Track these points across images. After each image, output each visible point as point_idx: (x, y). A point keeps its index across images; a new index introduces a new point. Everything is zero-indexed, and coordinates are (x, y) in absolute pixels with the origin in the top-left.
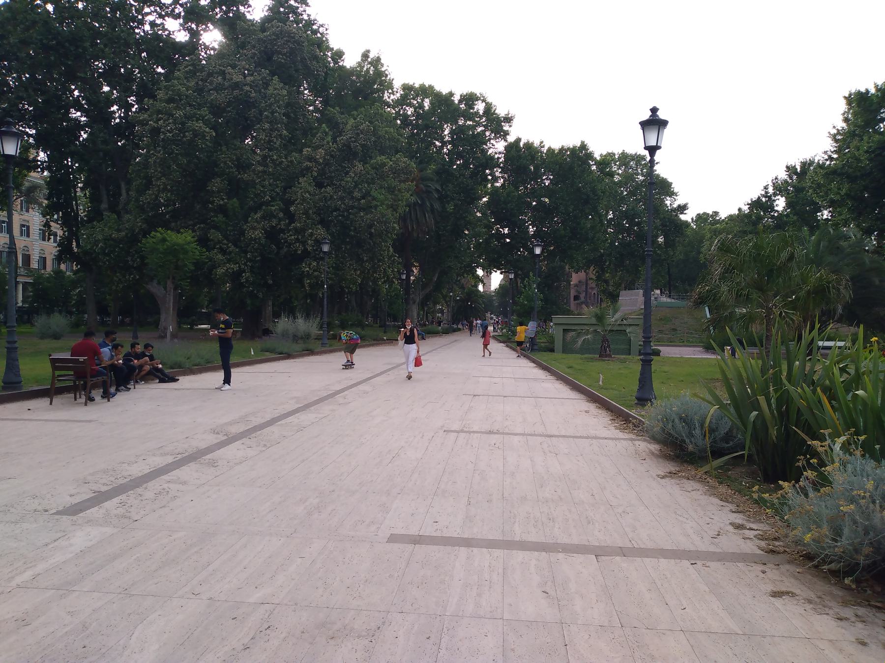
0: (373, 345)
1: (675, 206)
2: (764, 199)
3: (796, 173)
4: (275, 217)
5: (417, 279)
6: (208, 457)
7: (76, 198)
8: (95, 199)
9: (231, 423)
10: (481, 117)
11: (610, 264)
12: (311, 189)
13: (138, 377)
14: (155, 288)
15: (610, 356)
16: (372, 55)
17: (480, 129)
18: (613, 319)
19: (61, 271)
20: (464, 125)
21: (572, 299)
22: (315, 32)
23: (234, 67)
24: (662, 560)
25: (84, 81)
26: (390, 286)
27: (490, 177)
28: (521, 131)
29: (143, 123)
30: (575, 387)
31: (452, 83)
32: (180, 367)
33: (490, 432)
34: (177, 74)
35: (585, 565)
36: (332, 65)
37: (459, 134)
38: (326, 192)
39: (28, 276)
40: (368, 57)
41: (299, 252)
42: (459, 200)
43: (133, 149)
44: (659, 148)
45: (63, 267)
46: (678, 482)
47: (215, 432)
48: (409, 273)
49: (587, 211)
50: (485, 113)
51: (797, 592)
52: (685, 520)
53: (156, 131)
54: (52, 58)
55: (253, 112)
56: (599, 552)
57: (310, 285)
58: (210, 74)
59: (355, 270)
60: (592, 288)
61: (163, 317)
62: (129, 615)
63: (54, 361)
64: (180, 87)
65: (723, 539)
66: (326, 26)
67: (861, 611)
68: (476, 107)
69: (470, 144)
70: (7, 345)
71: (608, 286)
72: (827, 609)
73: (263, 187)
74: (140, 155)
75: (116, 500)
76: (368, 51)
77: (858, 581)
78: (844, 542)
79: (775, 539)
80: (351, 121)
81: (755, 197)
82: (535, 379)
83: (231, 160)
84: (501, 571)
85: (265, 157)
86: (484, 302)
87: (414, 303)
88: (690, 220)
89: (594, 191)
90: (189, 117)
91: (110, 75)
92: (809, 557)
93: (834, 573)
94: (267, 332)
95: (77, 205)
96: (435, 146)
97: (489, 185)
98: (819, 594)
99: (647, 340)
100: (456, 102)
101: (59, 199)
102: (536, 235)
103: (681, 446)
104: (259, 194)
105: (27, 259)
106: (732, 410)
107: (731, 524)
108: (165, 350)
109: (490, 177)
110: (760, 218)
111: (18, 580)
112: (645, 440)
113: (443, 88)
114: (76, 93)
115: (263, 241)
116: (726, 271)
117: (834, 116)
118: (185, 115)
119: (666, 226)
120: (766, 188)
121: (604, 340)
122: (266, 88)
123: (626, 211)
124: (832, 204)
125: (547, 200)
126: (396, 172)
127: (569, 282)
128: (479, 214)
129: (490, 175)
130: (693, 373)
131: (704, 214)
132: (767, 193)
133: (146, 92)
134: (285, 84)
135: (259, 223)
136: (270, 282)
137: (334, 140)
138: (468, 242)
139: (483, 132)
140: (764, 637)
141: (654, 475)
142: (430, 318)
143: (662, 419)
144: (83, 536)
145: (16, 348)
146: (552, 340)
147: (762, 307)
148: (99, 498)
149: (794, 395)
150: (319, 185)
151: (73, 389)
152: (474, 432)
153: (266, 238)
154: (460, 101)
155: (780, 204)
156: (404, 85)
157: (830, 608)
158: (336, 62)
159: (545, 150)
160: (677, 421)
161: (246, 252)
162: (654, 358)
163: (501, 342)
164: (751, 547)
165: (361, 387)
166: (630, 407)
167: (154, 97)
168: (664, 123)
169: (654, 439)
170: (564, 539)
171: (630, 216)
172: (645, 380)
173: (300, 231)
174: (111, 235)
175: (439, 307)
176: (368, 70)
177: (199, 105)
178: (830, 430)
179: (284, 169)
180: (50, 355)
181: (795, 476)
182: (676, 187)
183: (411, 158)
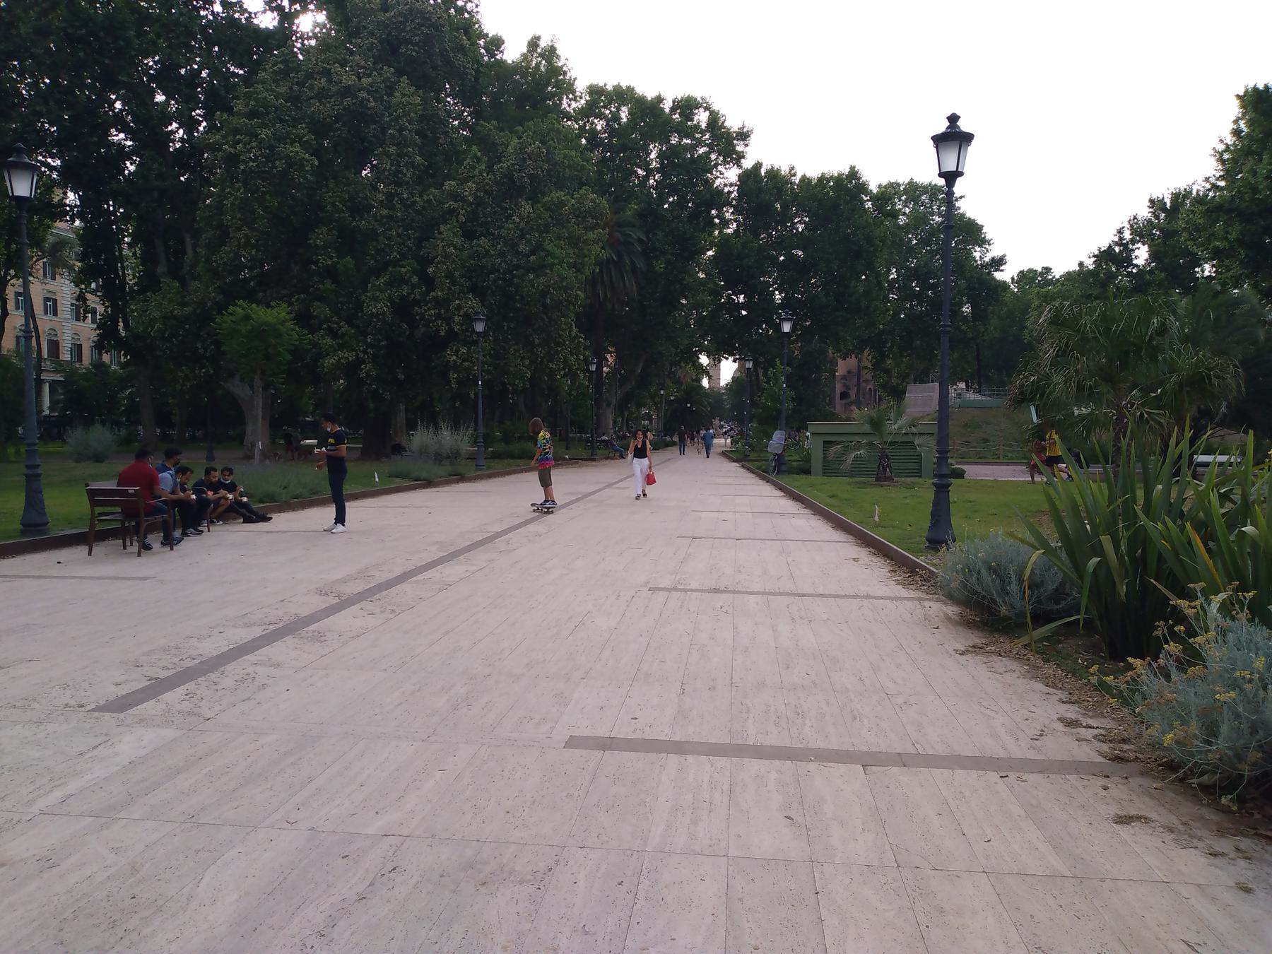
1: (987, 259)
3: (1164, 209)
4: (406, 282)
5: (614, 371)
7: (121, 259)
8: (148, 259)
9: (344, 581)
10: (703, 132)
11: (892, 346)
14: (238, 388)
15: (891, 479)
16: (543, 44)
17: (702, 150)
18: (894, 426)
19: (103, 364)
20: (679, 145)
23: (343, 64)
27: (717, 221)
28: (763, 152)
29: (213, 148)
30: (840, 525)
31: (661, 83)
33: (716, 591)
34: (262, 75)
35: (848, 778)
36: (486, 58)
38: (479, 245)
39: (57, 372)
40: (538, 46)
44: (961, 174)
45: (106, 358)
47: (321, 592)
48: (601, 361)
50: (709, 125)
51: (1153, 816)
52: (993, 714)
53: (232, 160)
54: (81, 54)
56: (868, 760)
57: (459, 382)
58: (309, 76)
59: (523, 359)
60: (867, 381)
61: (249, 429)
62: (197, 852)
63: (92, 494)
64: (266, 94)
65: (1048, 741)
67: (1245, 843)
68: (696, 118)
69: (688, 173)
71: (890, 377)
72: (1195, 841)
73: (388, 239)
74: (211, 195)
75: (180, 690)
76: (538, 38)
77: (1241, 800)
79: (1124, 741)
81: (1104, 245)
84: (726, 787)
85: (390, 196)
86: (709, 403)
87: (609, 405)
89: (869, 239)
90: (281, 139)
91: (166, 78)
92: (1172, 766)
94: (398, 449)
95: (123, 268)
96: (637, 176)
97: (716, 232)
99: (943, 457)
100: (667, 110)
101: (97, 261)
102: (785, 304)
103: (990, 608)
105: (55, 346)
106: (1064, 556)
107: (1059, 719)
108: (252, 476)
109: (717, 221)
110: (1112, 276)
112: (938, 600)
113: (647, 90)
115: (389, 318)
116: (1063, 353)
120: (1120, 232)
121: (883, 456)
122: (390, 95)
124: (1216, 255)
125: (800, 253)
127: (833, 372)
128: (701, 275)
129: (717, 217)
130: (1007, 503)
131: (1031, 270)
132: (1121, 239)
133: (217, 102)
134: (418, 88)
135: (382, 291)
136: (401, 377)
137: (490, 168)
138: (687, 316)
139: (707, 154)
140: (1103, 880)
141: (951, 651)
143: (963, 570)
144: (133, 741)
145: (39, 475)
146: (807, 459)
148: (156, 688)
150: (469, 235)
152: (692, 590)
154: (673, 110)
155: (1141, 254)
157: (1200, 839)
158: (493, 56)
159: (797, 179)
160: (984, 572)
161: (365, 334)
164: (1088, 753)
166: (917, 552)
167: (230, 110)
168: (968, 138)
169: (951, 598)
170: (820, 744)
171: (921, 275)
172: (940, 514)
174: (172, 312)
175: (644, 411)
176: (538, 65)
177: (294, 120)
179: (418, 212)
181: (1149, 649)
182: (988, 232)
183: (602, 192)
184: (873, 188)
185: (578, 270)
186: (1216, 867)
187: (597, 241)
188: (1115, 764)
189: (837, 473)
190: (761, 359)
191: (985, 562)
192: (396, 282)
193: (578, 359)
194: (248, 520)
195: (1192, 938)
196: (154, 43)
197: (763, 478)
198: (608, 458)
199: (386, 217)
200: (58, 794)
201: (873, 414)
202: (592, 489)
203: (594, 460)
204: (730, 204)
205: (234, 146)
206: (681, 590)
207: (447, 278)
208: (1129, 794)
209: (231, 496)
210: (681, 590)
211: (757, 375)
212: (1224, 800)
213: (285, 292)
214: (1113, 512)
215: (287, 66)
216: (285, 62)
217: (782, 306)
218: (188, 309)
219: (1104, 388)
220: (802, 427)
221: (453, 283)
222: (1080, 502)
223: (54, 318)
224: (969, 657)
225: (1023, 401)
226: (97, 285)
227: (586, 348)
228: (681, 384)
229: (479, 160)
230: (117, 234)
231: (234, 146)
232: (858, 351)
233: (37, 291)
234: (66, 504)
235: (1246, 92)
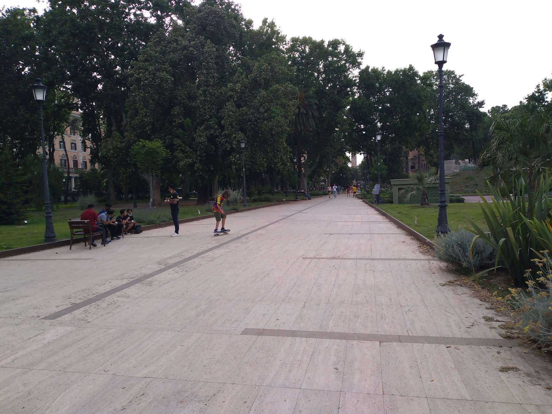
0: (276, 205)
2: (537, 94)
4: (212, 128)
8: (109, 125)
9: (171, 258)
11: (433, 144)
15: (428, 204)
16: (269, 21)
19: (95, 169)
21: (410, 168)
22: (233, 10)
23: (183, 36)
24: (426, 345)
28: (369, 61)
30: (400, 226)
31: (323, 35)
33: (334, 258)
35: (369, 349)
38: (243, 110)
40: (267, 22)
41: (228, 149)
44: (445, 62)
46: (453, 288)
47: (159, 263)
50: (345, 52)
51: (521, 367)
52: (451, 315)
53: (138, 80)
56: (382, 339)
57: (236, 169)
58: (169, 42)
59: (263, 158)
60: (423, 161)
63: (71, 224)
65: (475, 329)
66: (240, 5)
68: (339, 48)
69: (337, 72)
70: (46, 215)
72: (540, 381)
73: (204, 110)
75: (82, 309)
76: (267, 19)
80: (257, 64)
81: (530, 93)
84: (310, 353)
85: (204, 91)
86: (351, 174)
87: (304, 177)
89: (419, 97)
90: (158, 70)
91: (112, 48)
92: (534, 341)
101: (89, 126)
103: (458, 263)
104: (202, 115)
105: (76, 163)
106: (492, 239)
107: (483, 317)
110: (535, 107)
113: (317, 38)
115: (206, 143)
116: (501, 143)
118: (155, 69)
120: (538, 86)
121: (424, 194)
122: (203, 48)
127: (407, 158)
128: (345, 117)
129: (350, 91)
130: (476, 211)
131: (497, 107)
135: (203, 132)
136: (212, 169)
138: (339, 136)
139: (345, 63)
140: (487, 402)
142: (317, 185)
143: (445, 246)
147: (526, 165)
148: (75, 307)
149: (529, 225)
150: (239, 106)
151: (84, 240)
152: (322, 258)
153: (208, 141)
154: (328, 45)
156: (292, 38)
157: (543, 380)
158: (248, 28)
159: (385, 72)
161: (196, 151)
164: (494, 334)
165: (259, 232)
166: (432, 238)
167: (136, 59)
168: (448, 45)
169: (441, 259)
170: (363, 331)
172: (442, 220)
173: (228, 136)
176: (267, 30)
177: (164, 62)
179: (217, 98)
182: (476, 90)
184: (421, 74)
185: (286, 118)
186: (549, 395)
187: (294, 105)
188: (507, 340)
191: (456, 242)
192: (209, 128)
193: (287, 157)
197: (370, 206)
198: (303, 200)
199: (203, 100)
201: (418, 175)
203: (297, 201)
205: (138, 75)
206: (317, 258)
207: (229, 125)
208: (509, 356)
210: (317, 258)
211: (371, 162)
213: (163, 135)
215: (160, 39)
216: (159, 37)
219: (521, 158)
224: (446, 287)
227: (290, 152)
229: (242, 74)
231: (138, 75)
232: (418, 145)
233: (68, 140)
234: (62, 229)
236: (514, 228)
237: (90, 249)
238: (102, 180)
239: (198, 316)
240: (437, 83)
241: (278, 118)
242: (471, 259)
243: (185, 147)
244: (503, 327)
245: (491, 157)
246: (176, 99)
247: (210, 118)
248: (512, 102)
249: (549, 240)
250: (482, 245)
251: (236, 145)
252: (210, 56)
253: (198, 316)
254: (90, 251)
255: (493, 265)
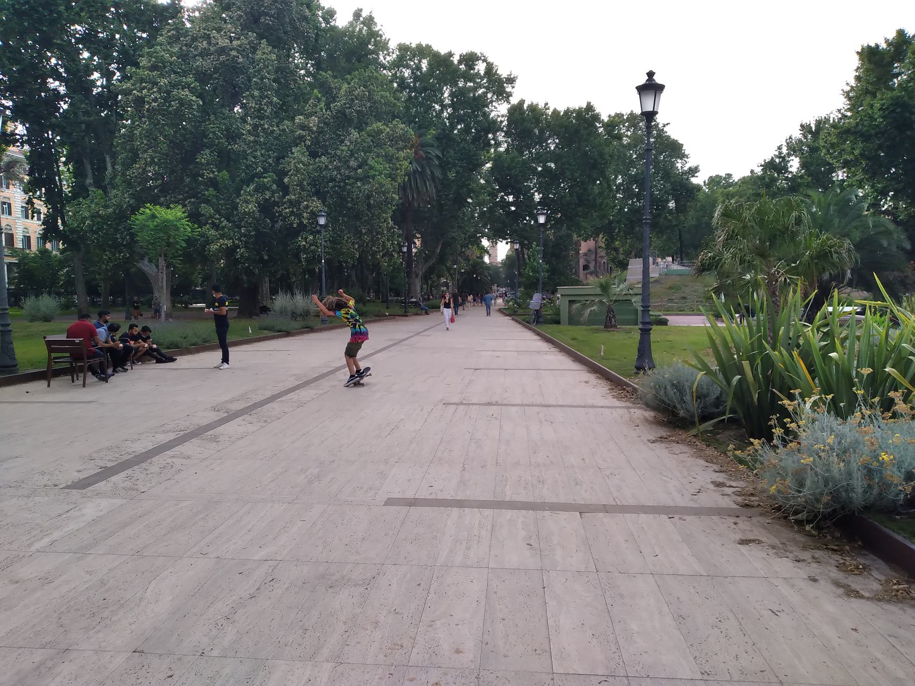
1: (686, 169)
3: (810, 132)
5: (420, 252)
6: (210, 433)
7: (59, 173)
8: (78, 173)
9: (231, 401)
11: (619, 232)
12: (305, 159)
13: (135, 358)
14: (146, 266)
15: (615, 326)
16: (364, 14)
17: (481, 91)
18: (617, 289)
19: (46, 251)
20: (464, 87)
23: (219, 30)
25: (61, 48)
26: (390, 260)
27: (493, 142)
28: (525, 93)
29: (127, 93)
31: (451, 43)
32: (177, 346)
33: (489, 404)
34: (160, 39)
35: (568, 521)
36: (323, 25)
37: (460, 97)
38: (320, 162)
39: (12, 256)
41: (295, 226)
42: (461, 166)
43: (117, 120)
45: (48, 246)
47: (215, 409)
48: (411, 243)
49: (595, 176)
50: (486, 73)
51: (764, 539)
52: (669, 480)
53: (140, 101)
54: (26, 24)
55: (241, 79)
56: (582, 509)
58: (194, 39)
60: (602, 257)
61: (156, 294)
62: (143, 573)
63: (49, 343)
64: (163, 53)
67: (818, 554)
68: (476, 67)
69: (471, 107)
71: (617, 254)
73: (255, 157)
74: (125, 126)
75: (122, 475)
76: (361, 10)
77: (818, 528)
78: (806, 491)
79: (752, 495)
82: (538, 352)
83: (221, 130)
84: (489, 527)
85: (255, 127)
86: (490, 275)
87: (417, 276)
88: (702, 184)
89: (601, 155)
90: (174, 86)
91: (88, 40)
92: (779, 509)
93: (800, 523)
94: (265, 310)
95: (60, 180)
97: (492, 150)
98: (784, 541)
100: (456, 62)
101: (41, 177)
105: (10, 238)
106: (721, 376)
108: (164, 329)
109: (493, 142)
110: (774, 180)
111: (37, 546)
113: (442, 49)
114: (53, 61)
117: (846, 71)
119: (677, 190)
120: (780, 148)
121: (610, 310)
122: (254, 53)
123: (637, 174)
124: (846, 164)
125: (553, 165)
126: (393, 140)
128: (482, 181)
129: (493, 139)
131: (717, 176)
132: (780, 153)
133: (128, 59)
134: (274, 47)
135: (252, 196)
136: (266, 257)
137: (328, 107)
139: (485, 94)
141: (645, 440)
142: (435, 292)
143: (655, 387)
144: (93, 508)
145: (10, 331)
146: (557, 313)
148: (106, 473)
150: (313, 155)
152: (473, 404)
153: (259, 211)
154: (460, 62)
155: (794, 164)
158: (328, 22)
159: (550, 112)
161: (239, 227)
162: (654, 327)
163: (507, 315)
164: (727, 503)
166: (629, 376)
167: (136, 65)
168: (660, 88)
169: (648, 406)
172: (644, 350)
174: (98, 212)
175: (443, 280)
176: (361, 30)
177: (184, 72)
178: (799, 391)
179: (276, 138)
180: (45, 338)
182: (687, 149)
189: (577, 323)
190: (526, 242)
191: (670, 381)
194: (159, 361)
195: (775, 609)
196: (78, 14)
198: (417, 314)
199: (253, 142)
200: (46, 541)
202: (405, 336)
203: (407, 316)
204: (503, 131)
206: (465, 404)
207: (297, 185)
208: (748, 527)
209: (146, 345)
210: (465, 404)
211: (523, 254)
212: (808, 528)
213: (181, 197)
214: (752, 343)
216: (177, 29)
217: (539, 203)
218: (110, 210)
220: (554, 292)
221: (303, 189)
222: (729, 339)
223: (9, 217)
224: (657, 444)
225: (703, 270)
226: (41, 193)
228: (469, 260)
229: (319, 100)
230: (55, 155)
231: (141, 91)
232: (595, 234)
235: (863, 49)
236: (752, 360)
237: (84, 386)
238: (61, 269)
239: (310, 482)
240: (629, 133)
241: (381, 179)
242: (694, 407)
243: (219, 219)
244: (739, 494)
245: (714, 258)
246: (206, 136)
247: (263, 173)
248: (739, 173)
249: (799, 378)
250: (705, 387)
251: (309, 219)
252: (266, 67)
253: (310, 482)
254: (84, 390)
255: (724, 414)
